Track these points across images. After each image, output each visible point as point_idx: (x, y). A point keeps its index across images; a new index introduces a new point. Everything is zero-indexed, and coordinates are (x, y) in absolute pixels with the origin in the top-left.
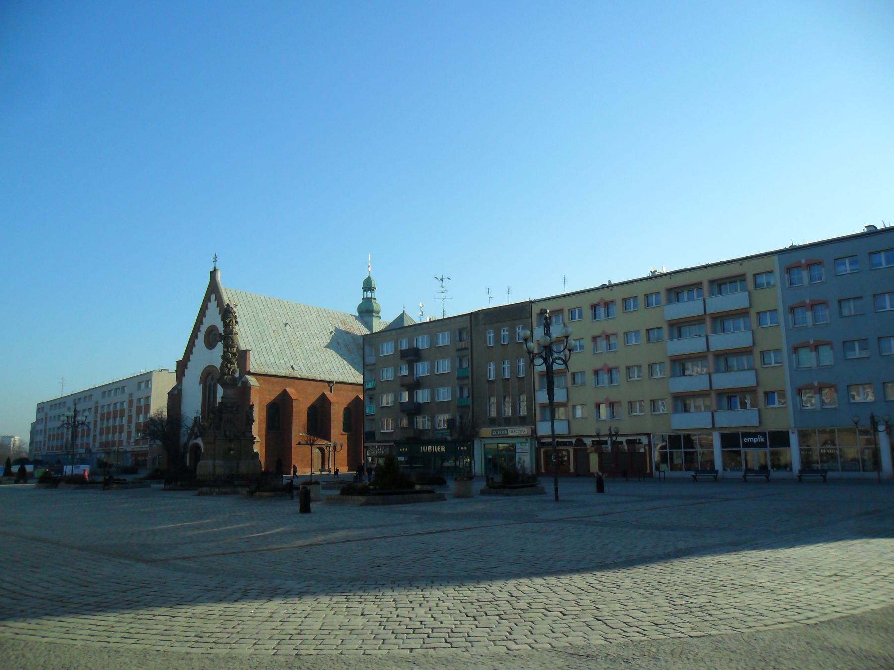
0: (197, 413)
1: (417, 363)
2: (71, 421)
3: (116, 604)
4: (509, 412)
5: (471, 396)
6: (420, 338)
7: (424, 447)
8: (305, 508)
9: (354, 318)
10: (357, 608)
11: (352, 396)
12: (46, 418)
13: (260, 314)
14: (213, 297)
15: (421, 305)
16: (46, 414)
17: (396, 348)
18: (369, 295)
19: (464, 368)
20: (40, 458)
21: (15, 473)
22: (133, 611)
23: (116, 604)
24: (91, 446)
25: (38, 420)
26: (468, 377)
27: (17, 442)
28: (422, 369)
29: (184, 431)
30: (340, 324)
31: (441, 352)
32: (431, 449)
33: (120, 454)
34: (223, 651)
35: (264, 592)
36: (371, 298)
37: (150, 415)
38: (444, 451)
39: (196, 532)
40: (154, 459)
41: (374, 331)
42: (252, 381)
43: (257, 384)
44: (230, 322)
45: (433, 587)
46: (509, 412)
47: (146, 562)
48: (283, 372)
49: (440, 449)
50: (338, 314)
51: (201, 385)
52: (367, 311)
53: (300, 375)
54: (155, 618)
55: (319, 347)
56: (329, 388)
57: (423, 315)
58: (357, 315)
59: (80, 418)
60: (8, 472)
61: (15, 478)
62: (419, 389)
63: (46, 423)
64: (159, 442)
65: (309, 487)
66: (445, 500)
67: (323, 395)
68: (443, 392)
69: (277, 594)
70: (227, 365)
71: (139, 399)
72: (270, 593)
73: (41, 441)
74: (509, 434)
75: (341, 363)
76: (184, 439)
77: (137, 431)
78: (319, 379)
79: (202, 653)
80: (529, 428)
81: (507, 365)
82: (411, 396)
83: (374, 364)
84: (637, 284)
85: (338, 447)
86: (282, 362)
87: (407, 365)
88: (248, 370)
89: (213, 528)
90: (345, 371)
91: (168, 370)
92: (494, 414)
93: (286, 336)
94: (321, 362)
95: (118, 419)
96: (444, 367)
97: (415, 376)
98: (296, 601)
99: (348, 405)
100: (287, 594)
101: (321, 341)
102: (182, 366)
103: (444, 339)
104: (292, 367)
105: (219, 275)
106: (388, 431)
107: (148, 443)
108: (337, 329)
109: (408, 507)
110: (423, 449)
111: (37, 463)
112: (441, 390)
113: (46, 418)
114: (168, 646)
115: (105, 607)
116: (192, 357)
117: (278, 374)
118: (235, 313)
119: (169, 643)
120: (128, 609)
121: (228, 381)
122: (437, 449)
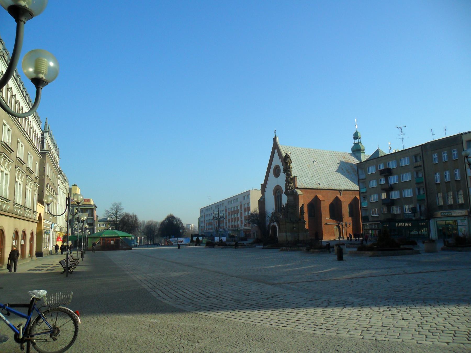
0: (273, 210)
1: (390, 177)
2: (217, 216)
3: (266, 305)
4: (451, 202)
5: (425, 194)
6: (391, 162)
7: (398, 224)
8: (340, 258)
9: (350, 154)
10: (398, 315)
11: (353, 197)
12: (204, 215)
13: (300, 157)
14: (276, 151)
15: (389, 144)
16: (204, 213)
17: (377, 169)
18: (357, 141)
19: (420, 177)
20: (203, 234)
21: (195, 241)
22: (276, 309)
23: (266, 305)
24: (225, 228)
25: (201, 216)
26: (422, 183)
27: (193, 227)
28: (393, 180)
29: (268, 219)
30: (343, 159)
31: (405, 169)
32: (402, 225)
33: (239, 231)
34: (333, 334)
35: (339, 303)
36: (359, 143)
37: (250, 212)
38: (411, 226)
39: (287, 270)
40: (254, 233)
41: (362, 161)
42: (299, 192)
43: (302, 194)
44: (288, 162)
45: (404, 304)
46: (451, 202)
47: (270, 284)
48: (315, 187)
49: (408, 225)
50: (341, 153)
51: (274, 195)
52: (357, 150)
53: (324, 187)
54: (288, 314)
55: (332, 171)
56: (340, 193)
57: (391, 149)
58: (352, 153)
59: (221, 215)
60: (192, 241)
61: (195, 243)
62: (393, 191)
63: (205, 217)
64: (256, 225)
65: (341, 246)
66: (420, 253)
67: (337, 197)
68: (407, 192)
69: (347, 304)
70: (288, 184)
71: (245, 205)
72: (344, 304)
73: (203, 226)
74: (452, 215)
75: (345, 179)
76: (268, 223)
77: (245, 219)
78: (334, 189)
79: (322, 334)
80: (466, 211)
81: (447, 174)
82: (388, 195)
83: (364, 179)
84: (412, 149)
85: (348, 225)
86: (314, 181)
87: (384, 178)
88: (296, 186)
89: (295, 268)
90: (348, 184)
91: (257, 189)
92: (441, 203)
93: (314, 167)
94: (334, 180)
95: (236, 215)
96: (407, 177)
97: (390, 184)
98: (359, 309)
99: (351, 202)
100: (352, 305)
101: (333, 168)
102: (264, 187)
103: (405, 162)
104: (319, 183)
105: (278, 140)
106: (375, 215)
107: (251, 226)
108: (341, 162)
109: (399, 258)
110: (398, 225)
111: (203, 236)
112: (406, 191)
113: (204, 215)
114: (302, 329)
115: (262, 306)
116: (268, 182)
117: (312, 188)
118: (290, 158)
119: (302, 328)
120: (273, 308)
121: (290, 193)
122: (406, 224)
